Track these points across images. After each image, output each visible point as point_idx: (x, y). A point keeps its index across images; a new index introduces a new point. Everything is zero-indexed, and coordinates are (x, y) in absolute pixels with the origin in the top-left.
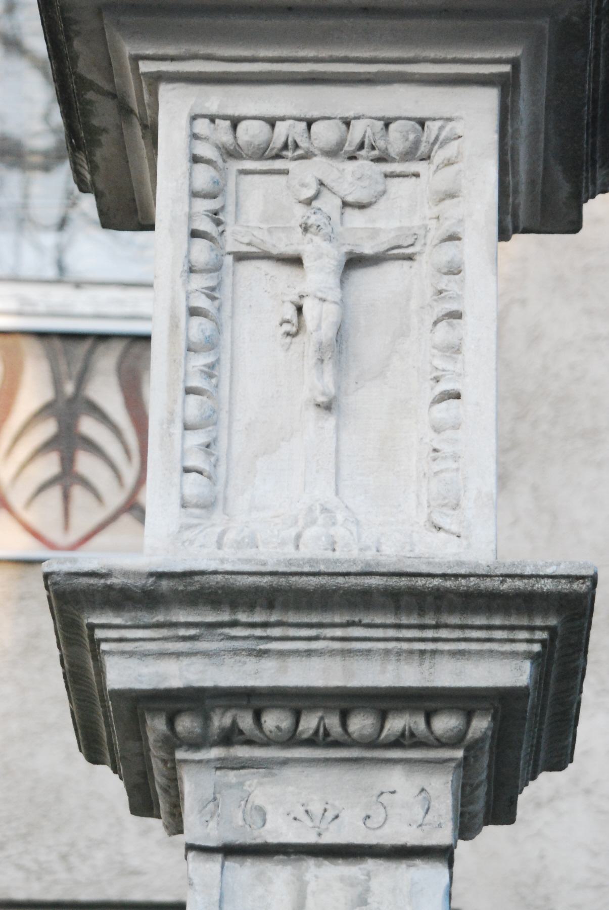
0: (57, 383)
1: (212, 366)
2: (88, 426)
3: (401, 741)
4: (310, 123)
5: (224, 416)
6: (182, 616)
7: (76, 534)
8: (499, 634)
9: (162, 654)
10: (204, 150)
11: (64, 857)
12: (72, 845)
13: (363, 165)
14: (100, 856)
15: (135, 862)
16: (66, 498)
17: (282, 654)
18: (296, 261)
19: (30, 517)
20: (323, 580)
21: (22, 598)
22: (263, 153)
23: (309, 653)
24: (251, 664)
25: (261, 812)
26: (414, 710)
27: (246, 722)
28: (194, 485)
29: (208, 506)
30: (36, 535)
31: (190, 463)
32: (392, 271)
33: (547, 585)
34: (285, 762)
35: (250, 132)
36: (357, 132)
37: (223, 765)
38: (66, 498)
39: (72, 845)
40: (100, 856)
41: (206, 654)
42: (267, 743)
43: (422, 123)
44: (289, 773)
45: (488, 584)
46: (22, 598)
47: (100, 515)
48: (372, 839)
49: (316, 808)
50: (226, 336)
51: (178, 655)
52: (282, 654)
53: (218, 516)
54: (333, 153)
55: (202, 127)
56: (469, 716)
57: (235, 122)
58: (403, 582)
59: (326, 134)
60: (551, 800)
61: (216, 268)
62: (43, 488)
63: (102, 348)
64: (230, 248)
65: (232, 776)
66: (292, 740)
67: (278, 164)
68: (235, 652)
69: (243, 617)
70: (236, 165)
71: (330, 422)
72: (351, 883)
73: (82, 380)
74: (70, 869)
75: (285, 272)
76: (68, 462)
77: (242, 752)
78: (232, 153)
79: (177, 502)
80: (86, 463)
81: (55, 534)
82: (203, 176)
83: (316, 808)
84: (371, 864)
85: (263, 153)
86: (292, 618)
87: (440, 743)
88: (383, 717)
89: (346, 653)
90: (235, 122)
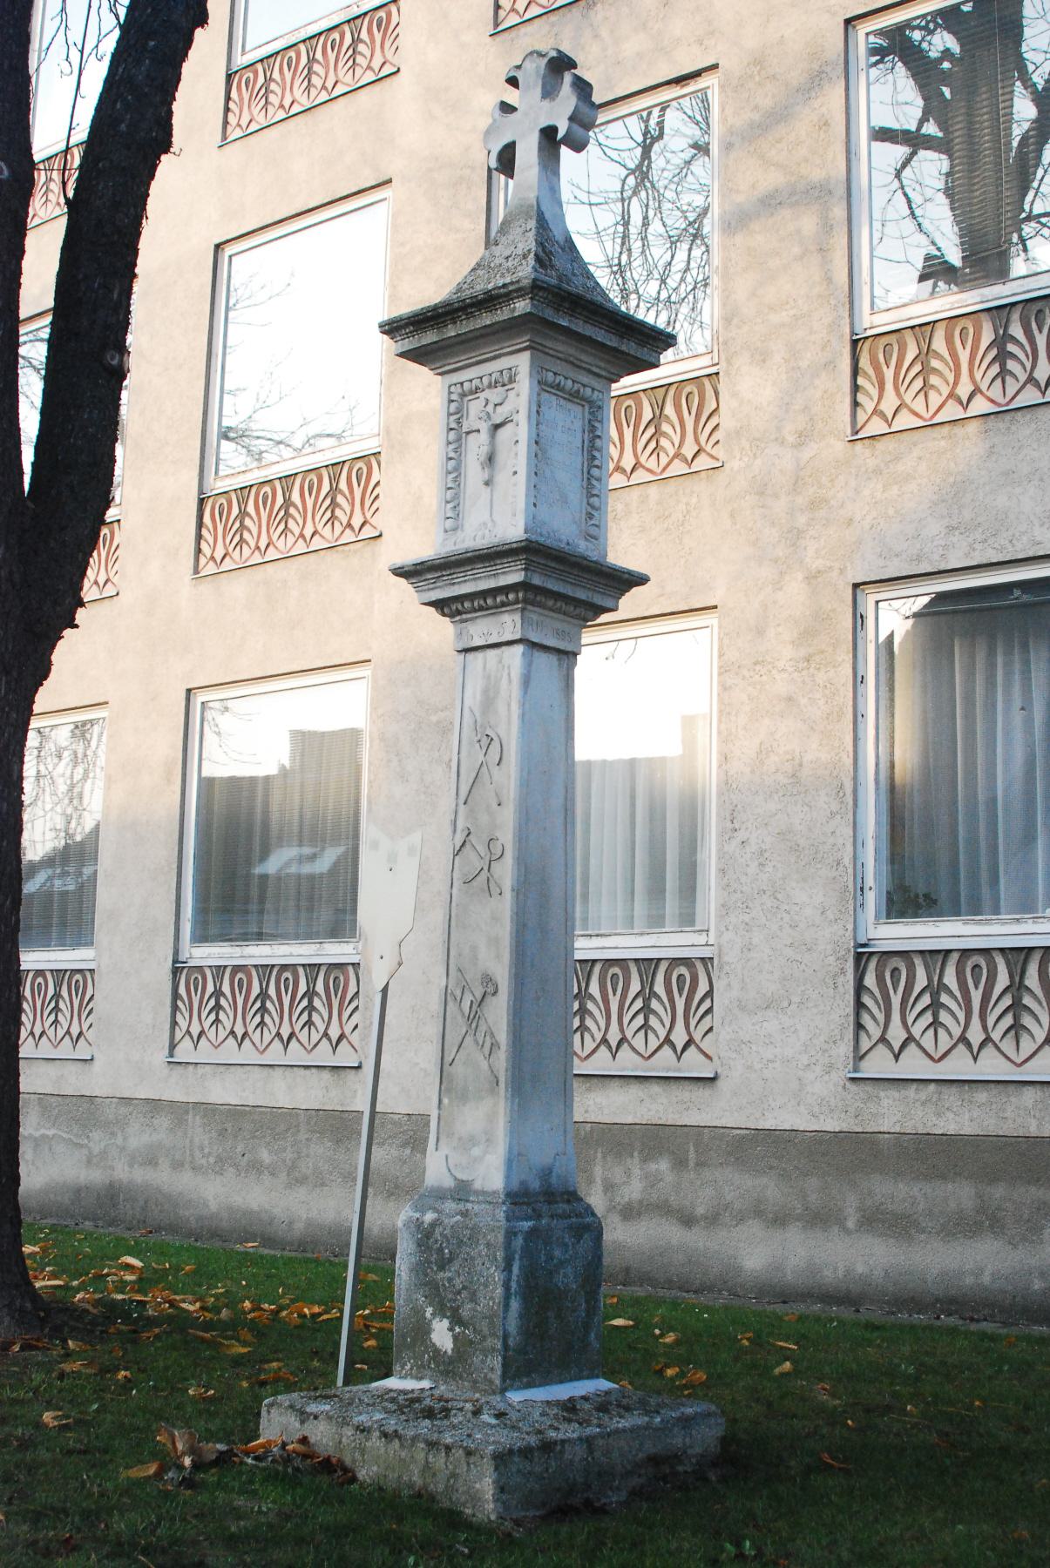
1: (456, 477)
2: (1011, 347)
4: (481, 378)
5: (462, 495)
7: (1008, 399)
8: (512, 564)
9: (429, 590)
10: (454, 397)
11: (1011, 541)
12: (1014, 535)
13: (500, 389)
14: (1025, 538)
15: (1038, 539)
16: (1004, 382)
17: (459, 583)
19: (988, 394)
20: (457, 557)
21: (986, 432)
23: (465, 581)
24: (453, 588)
26: (502, 594)
29: (455, 529)
30: (992, 401)
31: (448, 515)
32: (509, 427)
33: (515, 545)
34: (477, 617)
35: (467, 386)
36: (486, 381)
38: (1004, 382)
39: (1014, 535)
40: (1025, 538)
41: (439, 587)
43: (510, 369)
44: (478, 621)
45: (498, 549)
46: (986, 432)
51: (432, 589)
52: (459, 583)
53: (459, 532)
54: (490, 386)
56: (517, 592)
57: (462, 384)
58: (477, 553)
64: (464, 430)
67: (477, 395)
68: (446, 585)
69: (444, 573)
71: (489, 490)
73: (1006, 328)
74: (1013, 546)
77: (464, 616)
79: (442, 530)
81: (1001, 400)
85: (472, 392)
86: (458, 570)
89: (475, 579)
90: (462, 384)
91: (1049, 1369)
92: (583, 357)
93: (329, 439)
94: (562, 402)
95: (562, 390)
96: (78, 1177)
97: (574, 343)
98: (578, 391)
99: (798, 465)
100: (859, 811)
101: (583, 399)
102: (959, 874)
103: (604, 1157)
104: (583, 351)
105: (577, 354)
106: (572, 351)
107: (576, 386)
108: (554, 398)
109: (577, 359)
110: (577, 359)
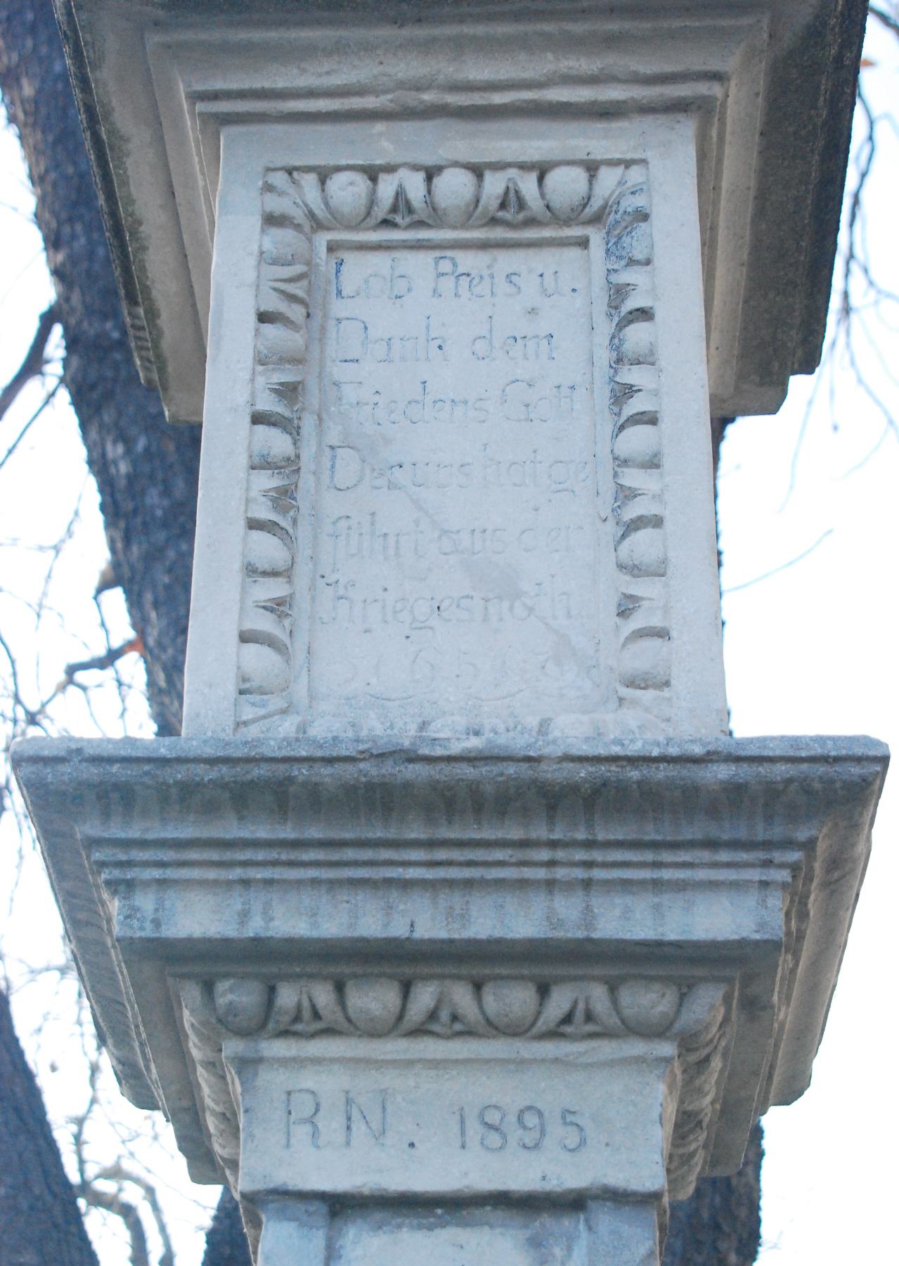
91: (840, 2)
92: (478, 70)
93: (271, 581)
94: (468, 261)
95: (434, 216)
96: (651, 753)
97: (385, 32)
98: (506, 200)
99: (682, 997)
100: (871, 163)
101: (555, 217)
102: (719, 202)
103: (781, 938)
104: (459, 46)
105: (444, 68)
106: (408, 67)
107: (494, 185)
108: (424, 260)
109: (455, 88)
110: (455, 88)
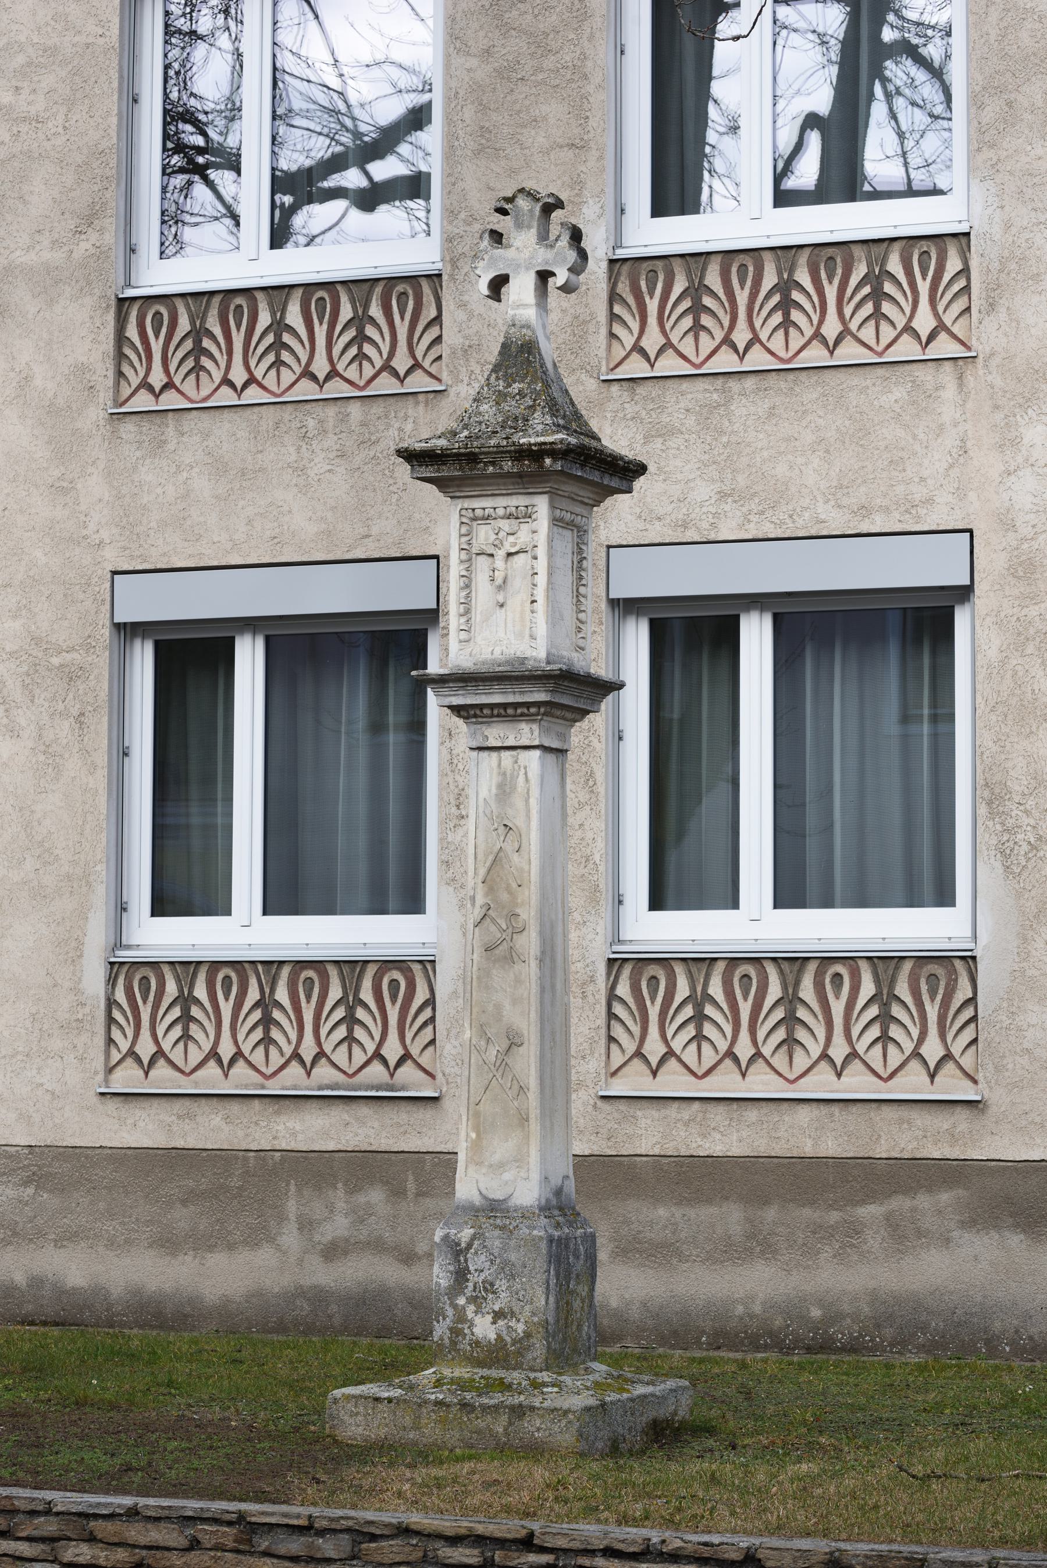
0: (780, 273)
3: (522, 715)
6: (451, 685)
10: (464, 520)
11: (791, 516)
13: (513, 521)
15: (823, 517)
16: (787, 334)
18: (492, 555)
22: (483, 518)
25: (487, 737)
27: (478, 712)
28: (463, 635)
37: (475, 723)
38: (787, 334)
42: (486, 717)
44: (494, 725)
47: (802, 341)
48: (517, 744)
49: (502, 735)
50: (473, 584)
55: (464, 512)
59: (501, 512)
60: (1015, 471)
61: (470, 560)
62: (775, 330)
63: (800, 251)
65: (479, 726)
66: (492, 716)
70: (475, 523)
72: (513, 756)
75: (490, 559)
76: (787, 315)
77: (480, 720)
78: (475, 519)
80: (796, 315)
81: (782, 354)
82: (464, 530)
83: (502, 735)
84: (519, 751)
87: (533, 715)
88: (516, 709)
90: (473, 510)
